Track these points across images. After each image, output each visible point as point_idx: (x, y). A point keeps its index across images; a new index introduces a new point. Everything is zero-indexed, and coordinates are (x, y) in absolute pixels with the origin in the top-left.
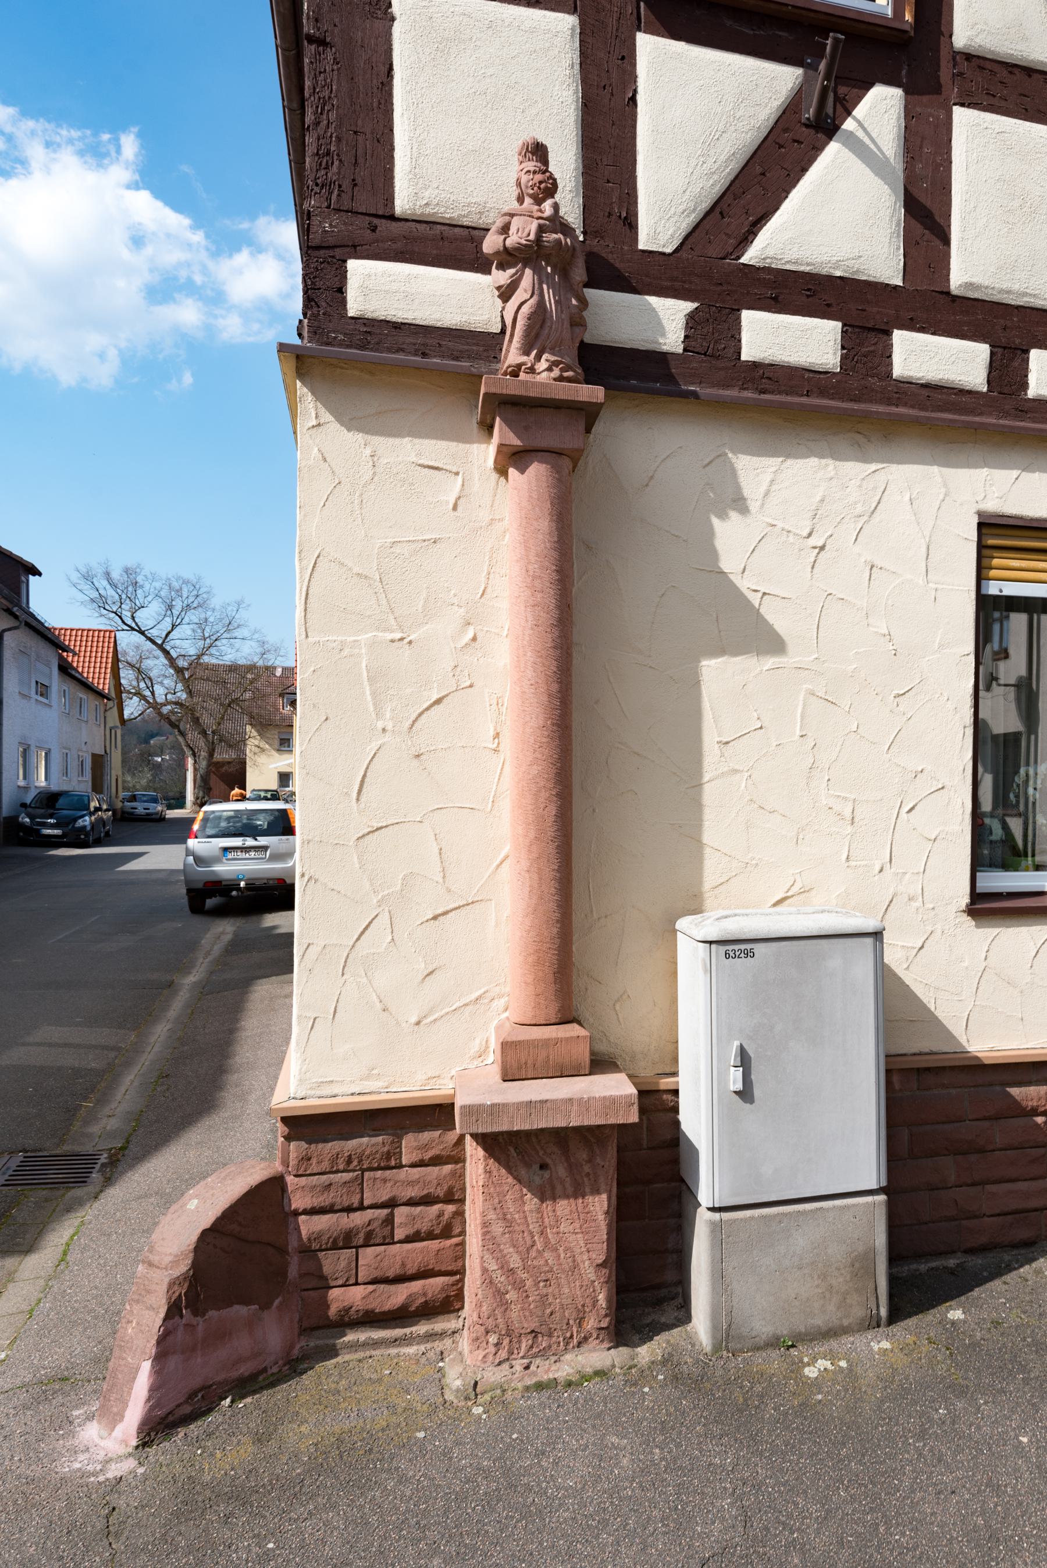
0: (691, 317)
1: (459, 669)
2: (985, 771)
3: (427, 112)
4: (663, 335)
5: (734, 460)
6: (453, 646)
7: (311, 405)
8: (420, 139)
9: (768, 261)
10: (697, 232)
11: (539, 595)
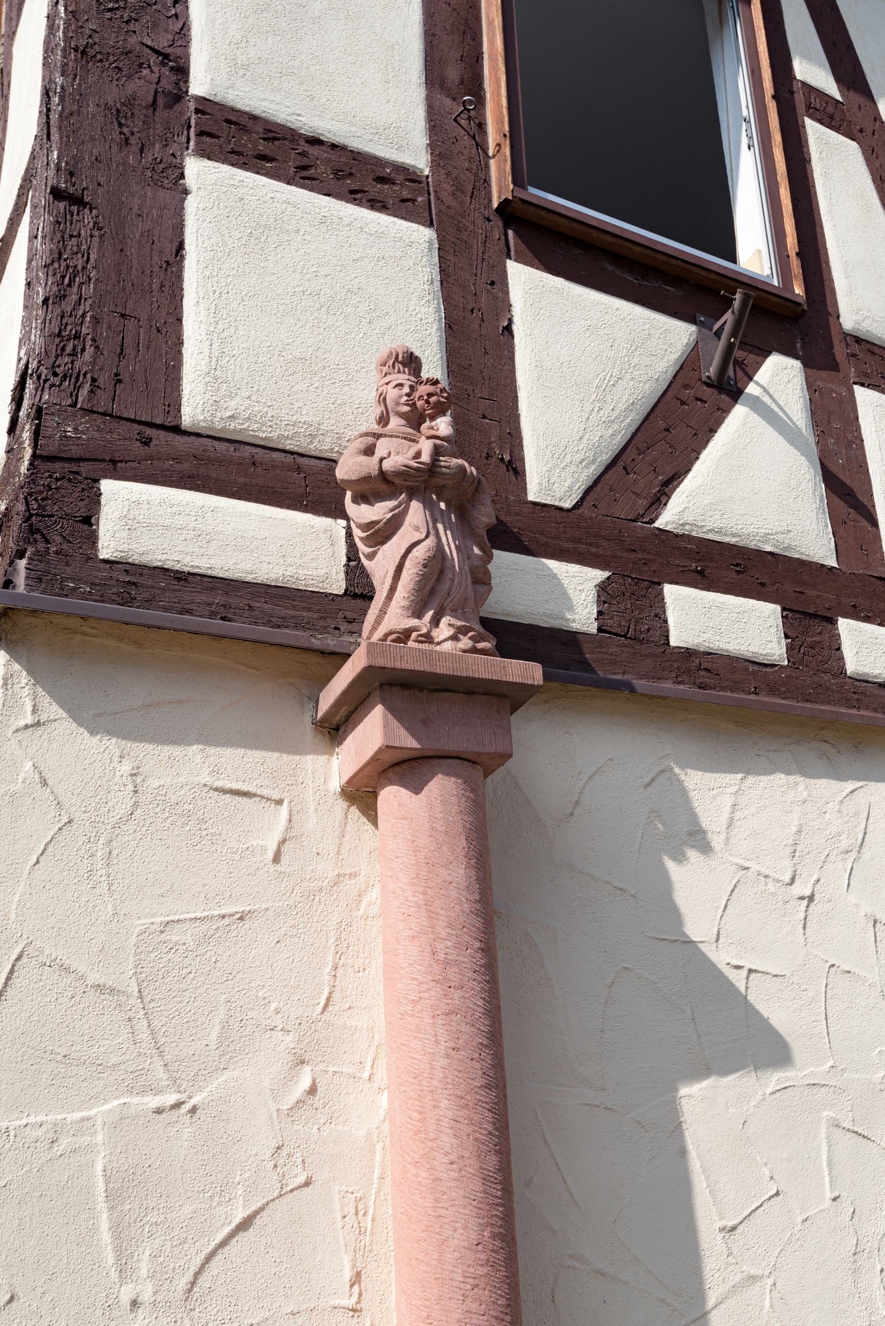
0: (603, 588)
1: (284, 1153)
3: (234, 305)
4: (571, 609)
5: (683, 777)
6: (273, 1108)
7: (26, 691)
8: (223, 336)
9: (687, 527)
10: (600, 486)
11: (457, 994)
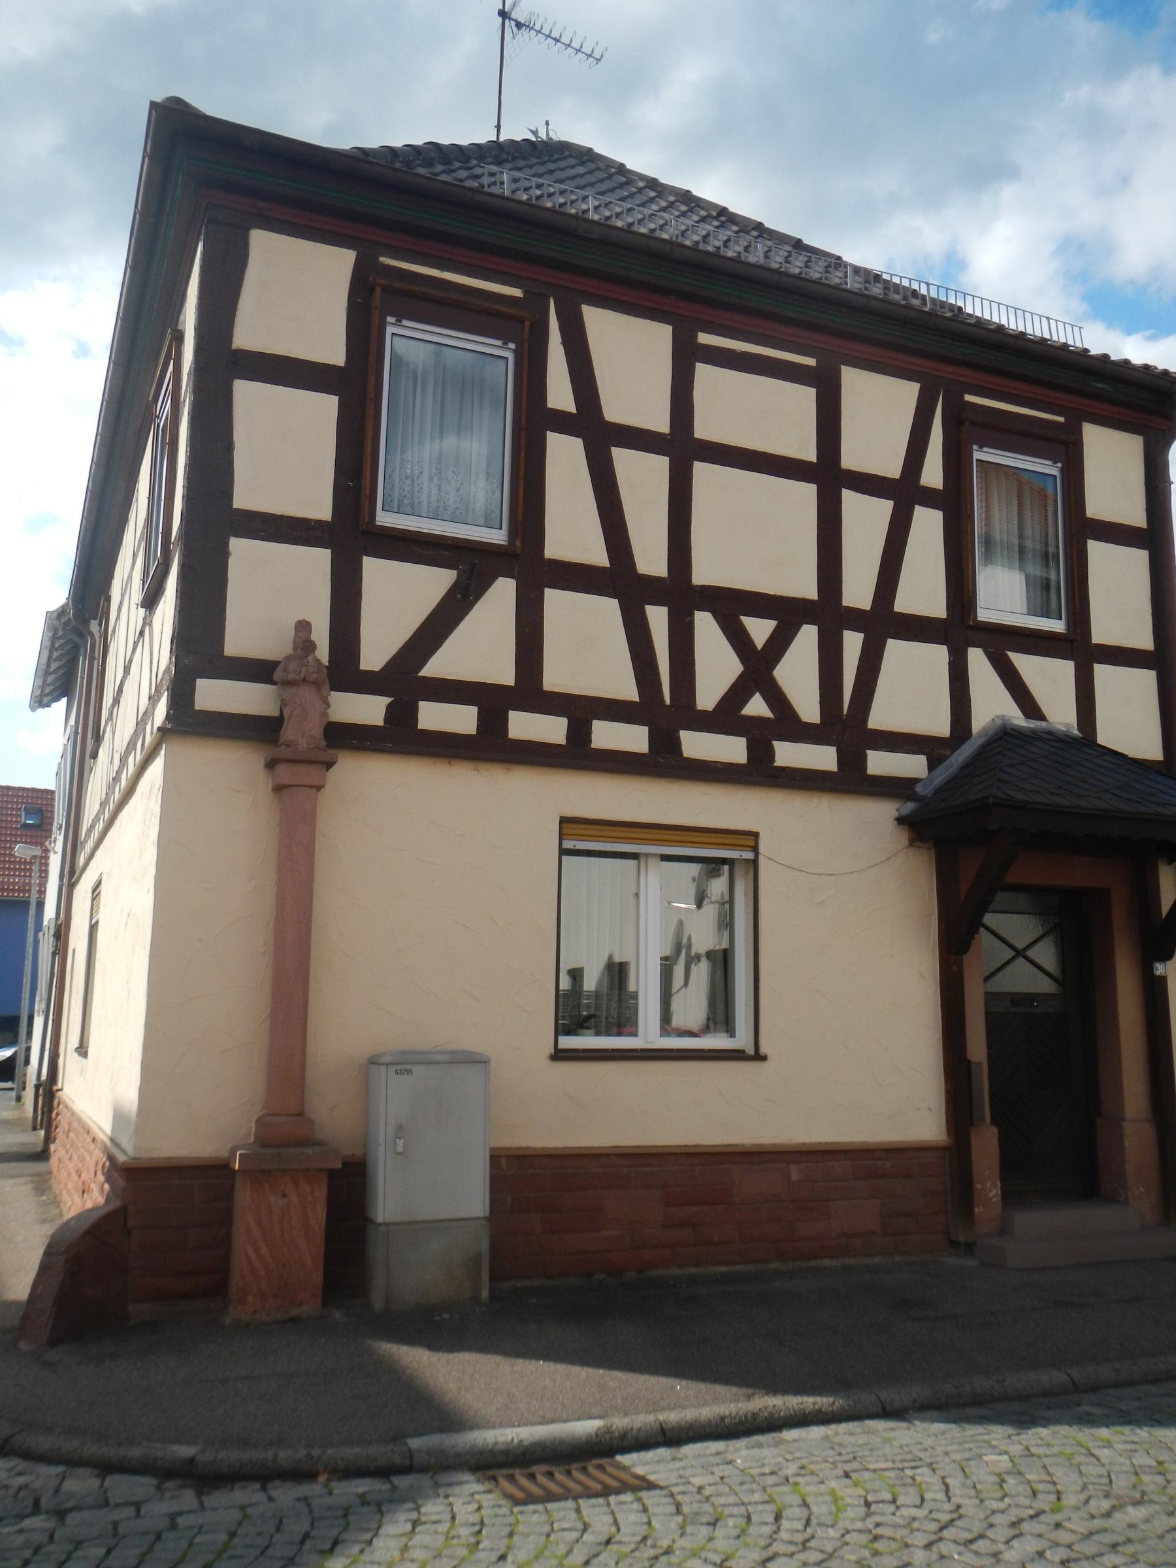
2: (979, 1064)
